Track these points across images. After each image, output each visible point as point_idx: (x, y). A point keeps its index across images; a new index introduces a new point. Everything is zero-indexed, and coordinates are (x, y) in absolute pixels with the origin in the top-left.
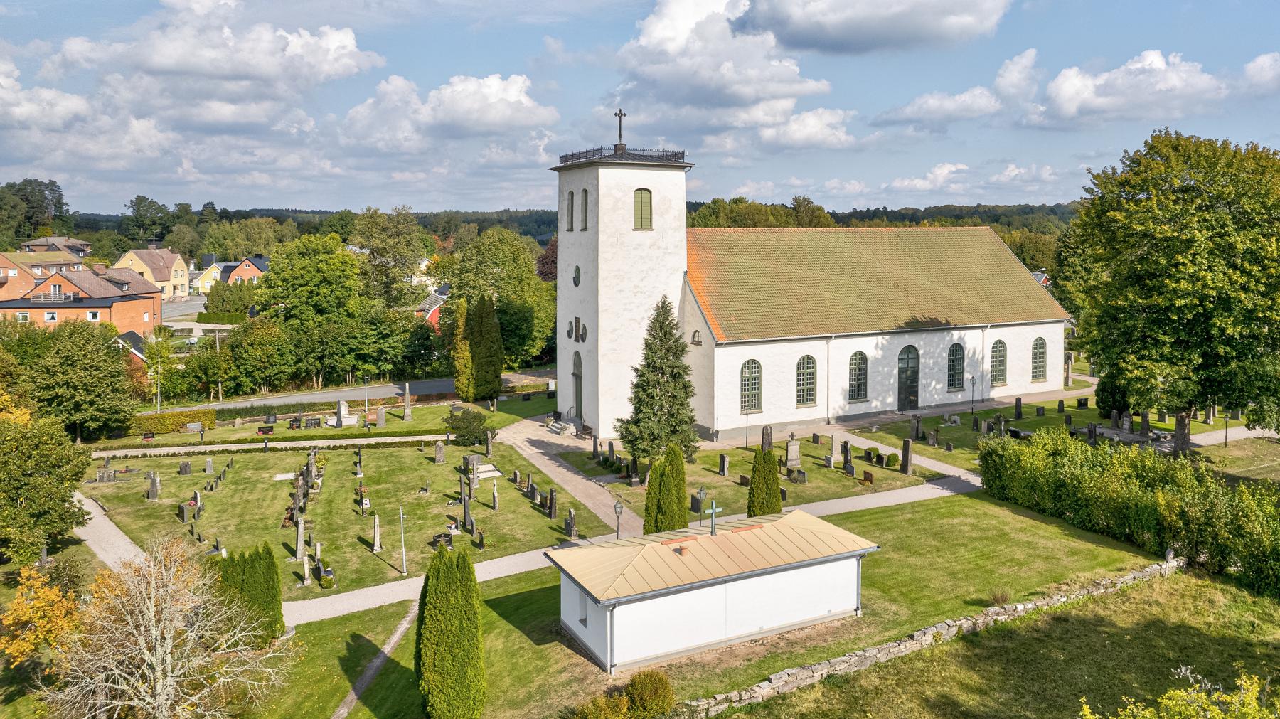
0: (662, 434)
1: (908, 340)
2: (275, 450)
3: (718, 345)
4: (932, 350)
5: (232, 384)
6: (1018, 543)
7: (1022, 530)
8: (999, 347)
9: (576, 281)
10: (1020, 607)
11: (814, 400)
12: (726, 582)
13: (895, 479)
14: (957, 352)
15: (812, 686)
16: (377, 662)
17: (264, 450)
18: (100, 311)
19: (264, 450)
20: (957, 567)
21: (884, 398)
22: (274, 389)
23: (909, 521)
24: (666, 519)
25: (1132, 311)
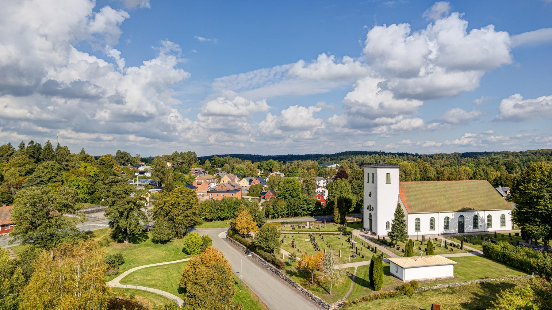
0: (399, 236)
1: (461, 214)
2: (300, 233)
3: (409, 214)
4: (469, 218)
5: (273, 215)
6: (493, 268)
7: (494, 265)
8: (490, 217)
9: (370, 195)
10: (492, 280)
11: (434, 229)
12: (425, 267)
13: (459, 251)
14: (476, 218)
15: (445, 288)
16: (354, 277)
17: (298, 233)
18: (233, 194)
19: (298, 233)
20: (476, 271)
21: (454, 229)
22: (282, 217)
23: (463, 260)
24: (410, 254)
25: (527, 212)
